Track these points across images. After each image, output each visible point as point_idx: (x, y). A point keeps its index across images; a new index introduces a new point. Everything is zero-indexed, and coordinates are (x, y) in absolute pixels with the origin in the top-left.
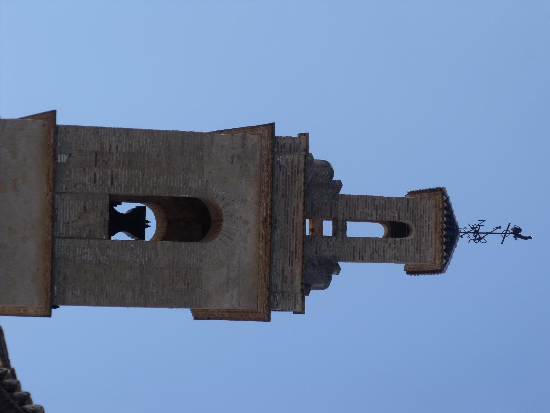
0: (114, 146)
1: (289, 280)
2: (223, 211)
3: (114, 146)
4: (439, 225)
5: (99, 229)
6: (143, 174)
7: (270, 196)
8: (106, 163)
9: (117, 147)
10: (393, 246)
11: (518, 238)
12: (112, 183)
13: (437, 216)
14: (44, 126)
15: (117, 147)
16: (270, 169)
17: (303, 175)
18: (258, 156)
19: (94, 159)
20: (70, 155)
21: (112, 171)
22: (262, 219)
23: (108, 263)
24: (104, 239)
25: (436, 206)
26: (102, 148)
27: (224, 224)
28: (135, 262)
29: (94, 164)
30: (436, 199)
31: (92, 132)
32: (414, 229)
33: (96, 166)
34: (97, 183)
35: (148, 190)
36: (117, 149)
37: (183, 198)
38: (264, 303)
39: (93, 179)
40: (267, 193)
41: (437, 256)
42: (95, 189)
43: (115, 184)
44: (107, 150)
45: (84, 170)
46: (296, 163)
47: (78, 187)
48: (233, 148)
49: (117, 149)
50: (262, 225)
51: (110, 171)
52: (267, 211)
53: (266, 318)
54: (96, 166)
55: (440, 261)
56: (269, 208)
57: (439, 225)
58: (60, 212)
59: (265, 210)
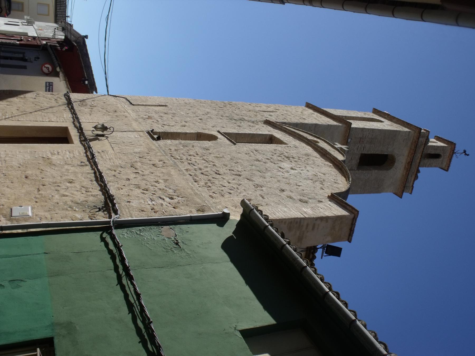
0: (367, 135)
1: (409, 182)
2: (396, 159)
3: (367, 135)
4: (450, 156)
5: (354, 166)
6: (374, 146)
7: (413, 155)
8: (363, 142)
9: (368, 136)
10: (435, 162)
11: (466, 155)
12: (363, 150)
13: (450, 152)
14: (345, 128)
15: (368, 136)
16: (416, 145)
17: (424, 145)
18: (412, 139)
19: (359, 140)
20: (351, 139)
21: (364, 145)
22: (408, 162)
23: (355, 179)
24: (355, 170)
25: (451, 149)
26: (363, 136)
27: (396, 164)
28: (364, 178)
29: (359, 142)
30: (452, 147)
31: (361, 130)
32: (443, 156)
33: (359, 143)
34: (358, 150)
35: (375, 152)
36: (368, 137)
37: (385, 154)
38: (401, 191)
39: (357, 148)
40: (412, 153)
41: (447, 166)
42: (357, 152)
43: (364, 150)
44: (365, 137)
45: (355, 145)
46: (422, 141)
47: (352, 151)
48: (405, 136)
49: (368, 137)
50: (407, 164)
51: (364, 145)
52: (410, 160)
53: (401, 197)
54: (359, 143)
55: (448, 168)
56: (412, 159)
57: (450, 156)
58: (264, 110)
59: (409, 159)
